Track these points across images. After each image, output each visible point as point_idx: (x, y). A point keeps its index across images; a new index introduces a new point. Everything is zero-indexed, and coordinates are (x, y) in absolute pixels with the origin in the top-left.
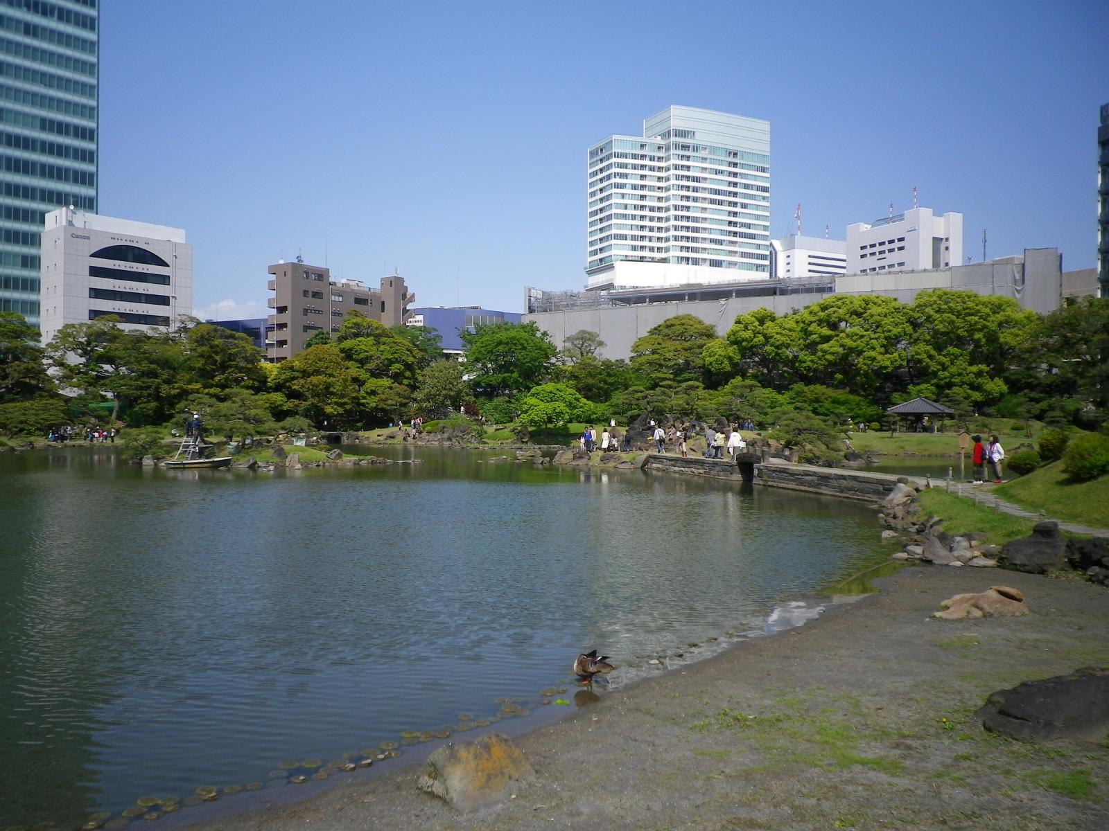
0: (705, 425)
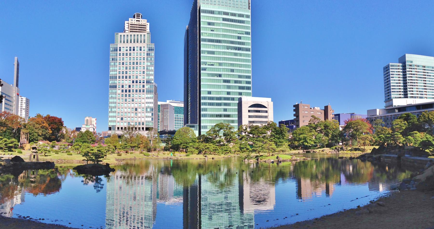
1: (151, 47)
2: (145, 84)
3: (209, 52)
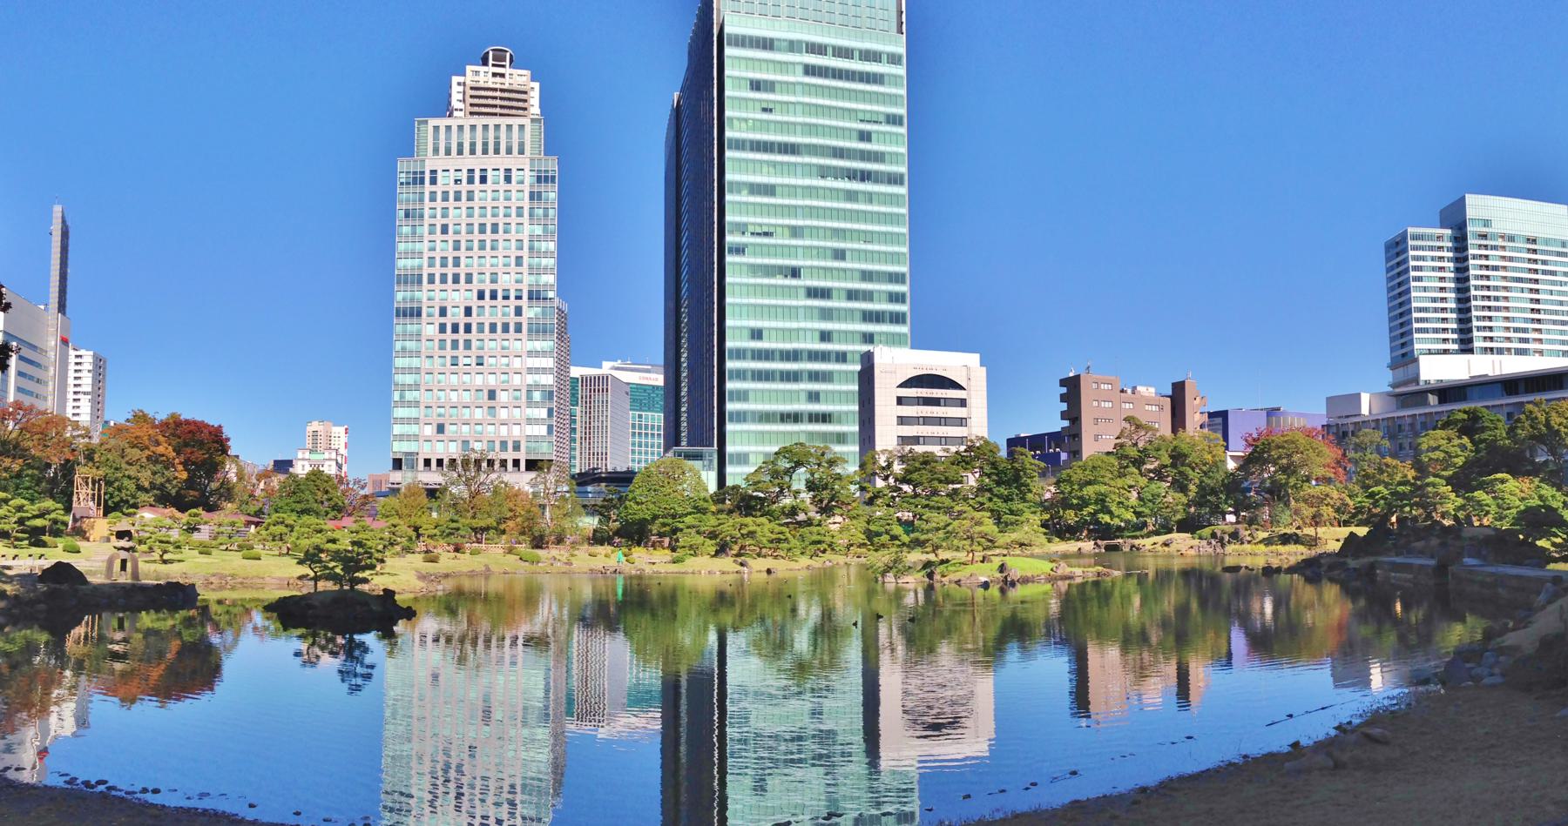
0: (1312, 489)
1: (546, 171)
2: (524, 302)
3: (756, 189)
